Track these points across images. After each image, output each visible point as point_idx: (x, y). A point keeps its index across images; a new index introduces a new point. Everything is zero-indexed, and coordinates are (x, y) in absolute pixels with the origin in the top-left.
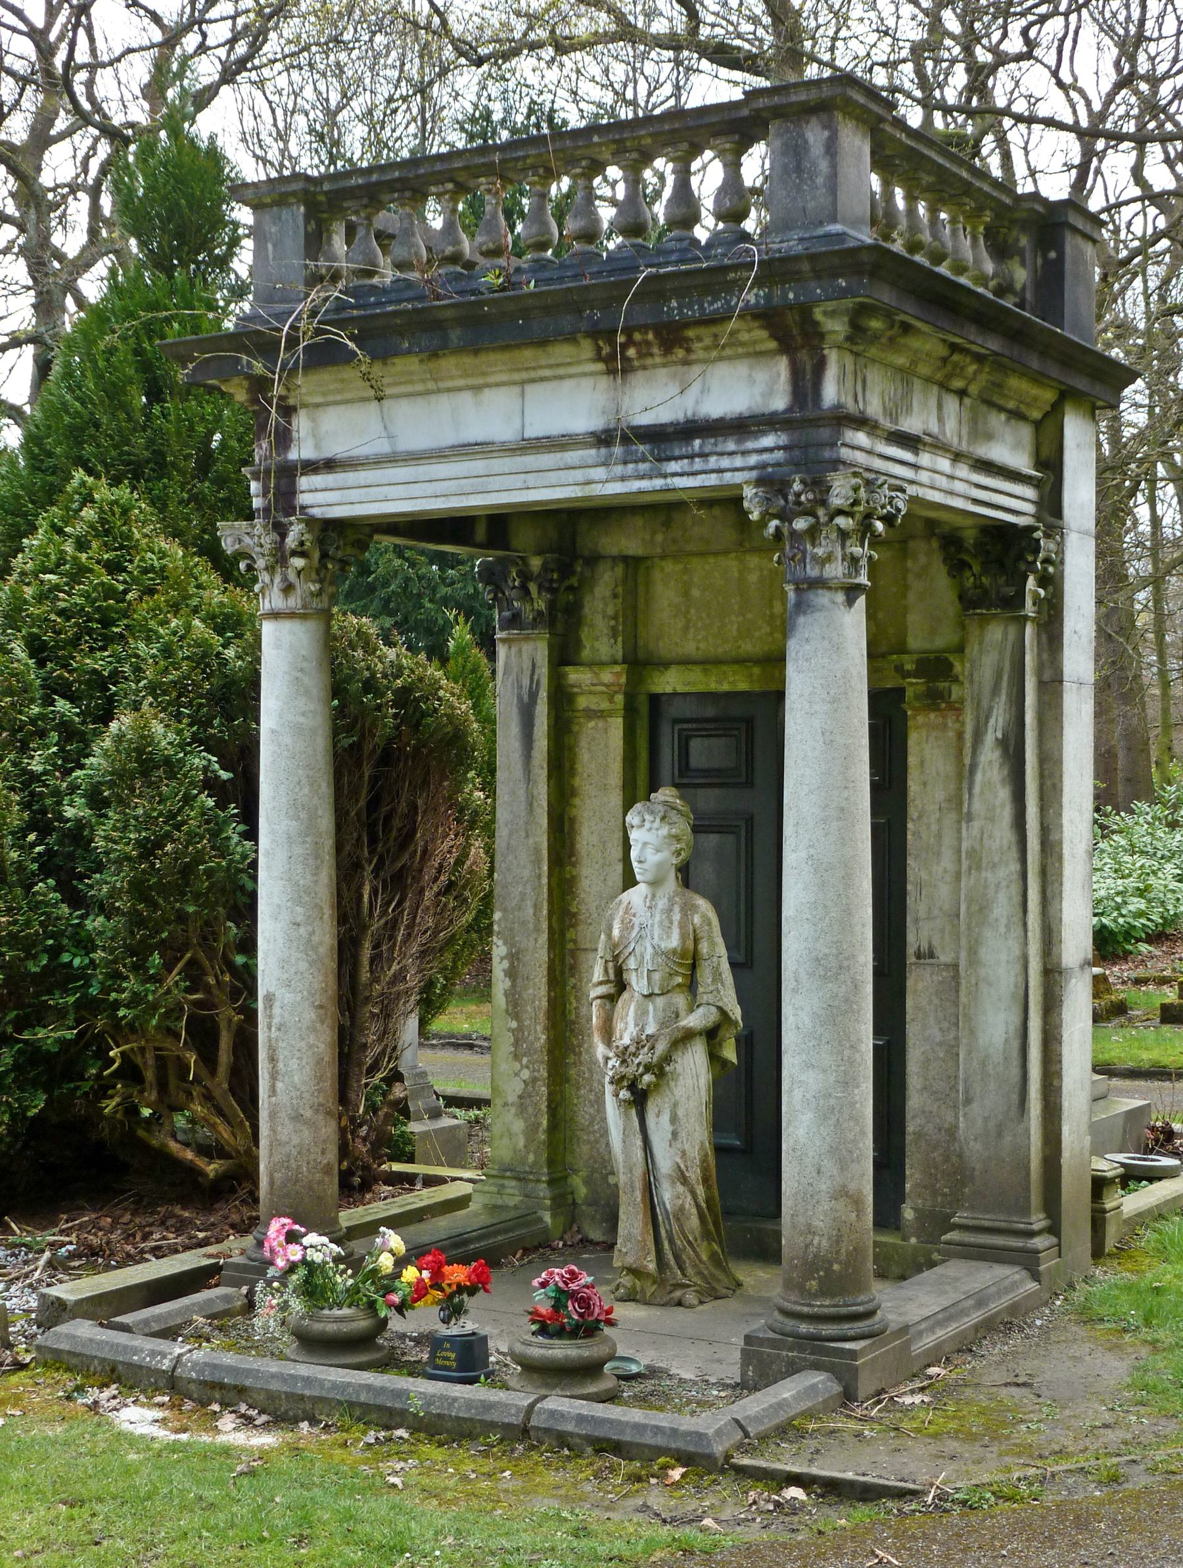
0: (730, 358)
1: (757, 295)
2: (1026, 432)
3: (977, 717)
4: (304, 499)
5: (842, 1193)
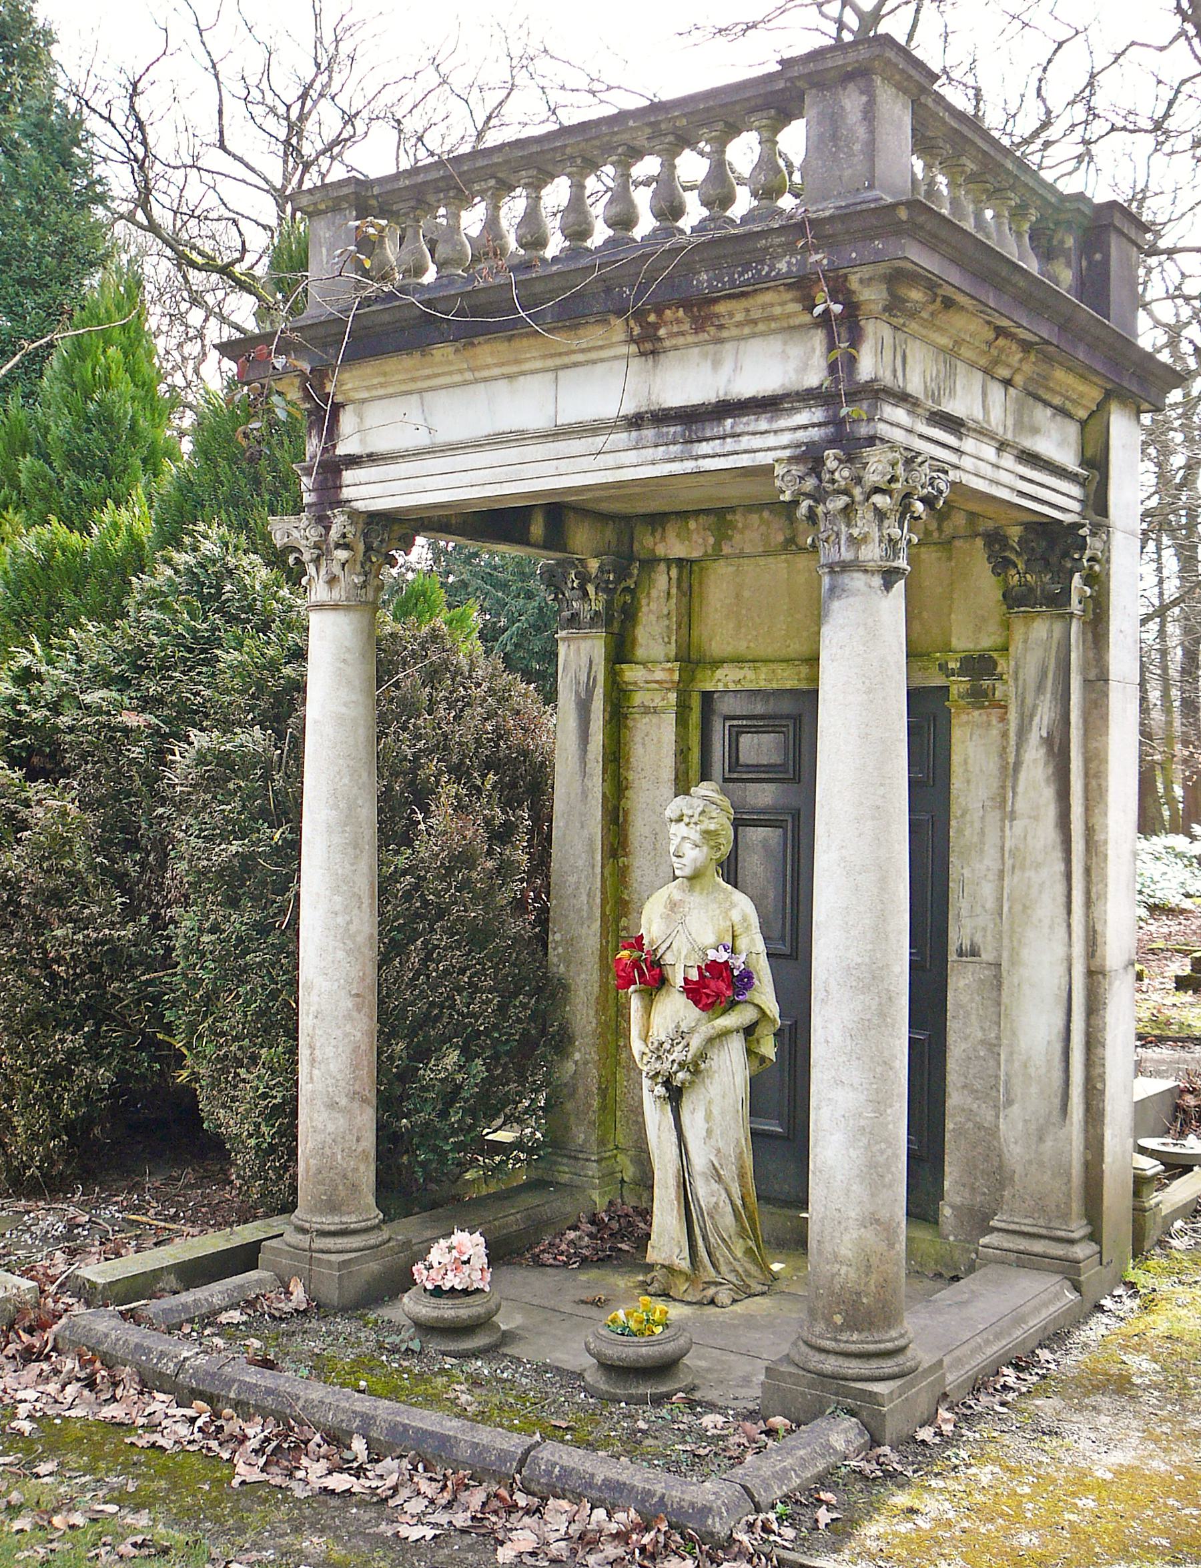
0: (763, 334)
1: (789, 263)
2: (1072, 429)
3: (1022, 715)
4: (346, 493)
5: (872, 1220)
